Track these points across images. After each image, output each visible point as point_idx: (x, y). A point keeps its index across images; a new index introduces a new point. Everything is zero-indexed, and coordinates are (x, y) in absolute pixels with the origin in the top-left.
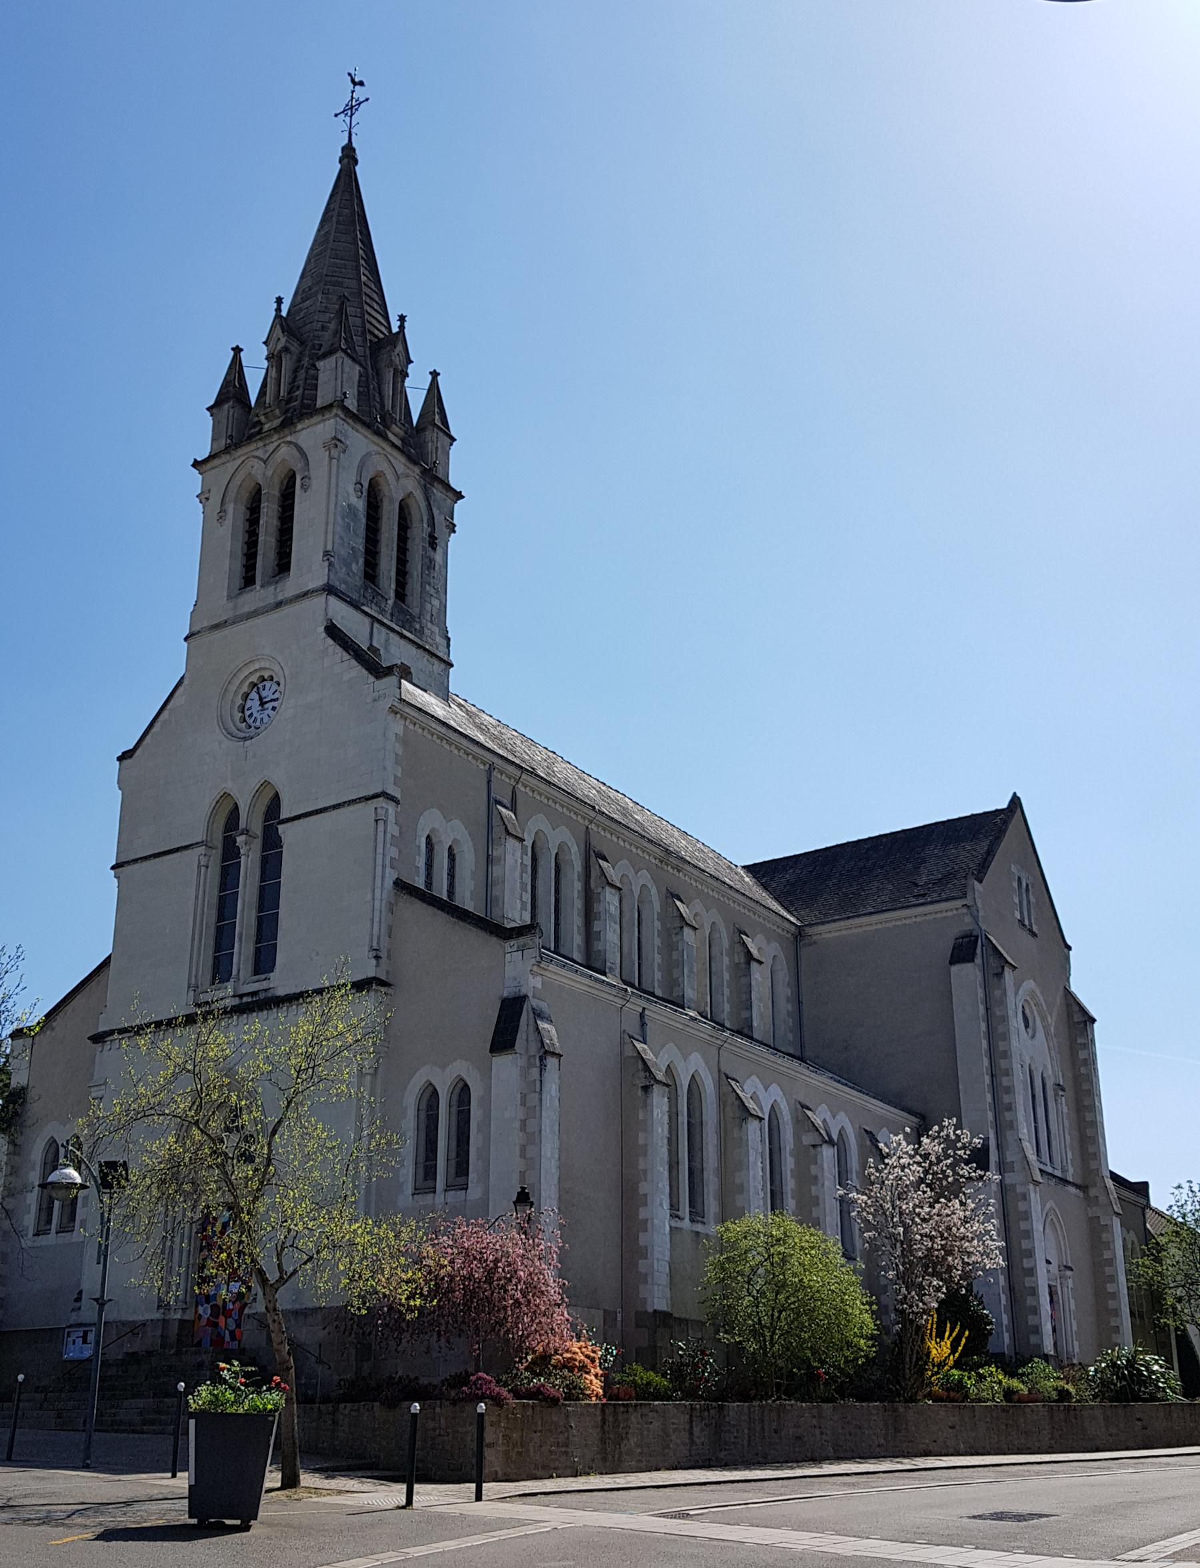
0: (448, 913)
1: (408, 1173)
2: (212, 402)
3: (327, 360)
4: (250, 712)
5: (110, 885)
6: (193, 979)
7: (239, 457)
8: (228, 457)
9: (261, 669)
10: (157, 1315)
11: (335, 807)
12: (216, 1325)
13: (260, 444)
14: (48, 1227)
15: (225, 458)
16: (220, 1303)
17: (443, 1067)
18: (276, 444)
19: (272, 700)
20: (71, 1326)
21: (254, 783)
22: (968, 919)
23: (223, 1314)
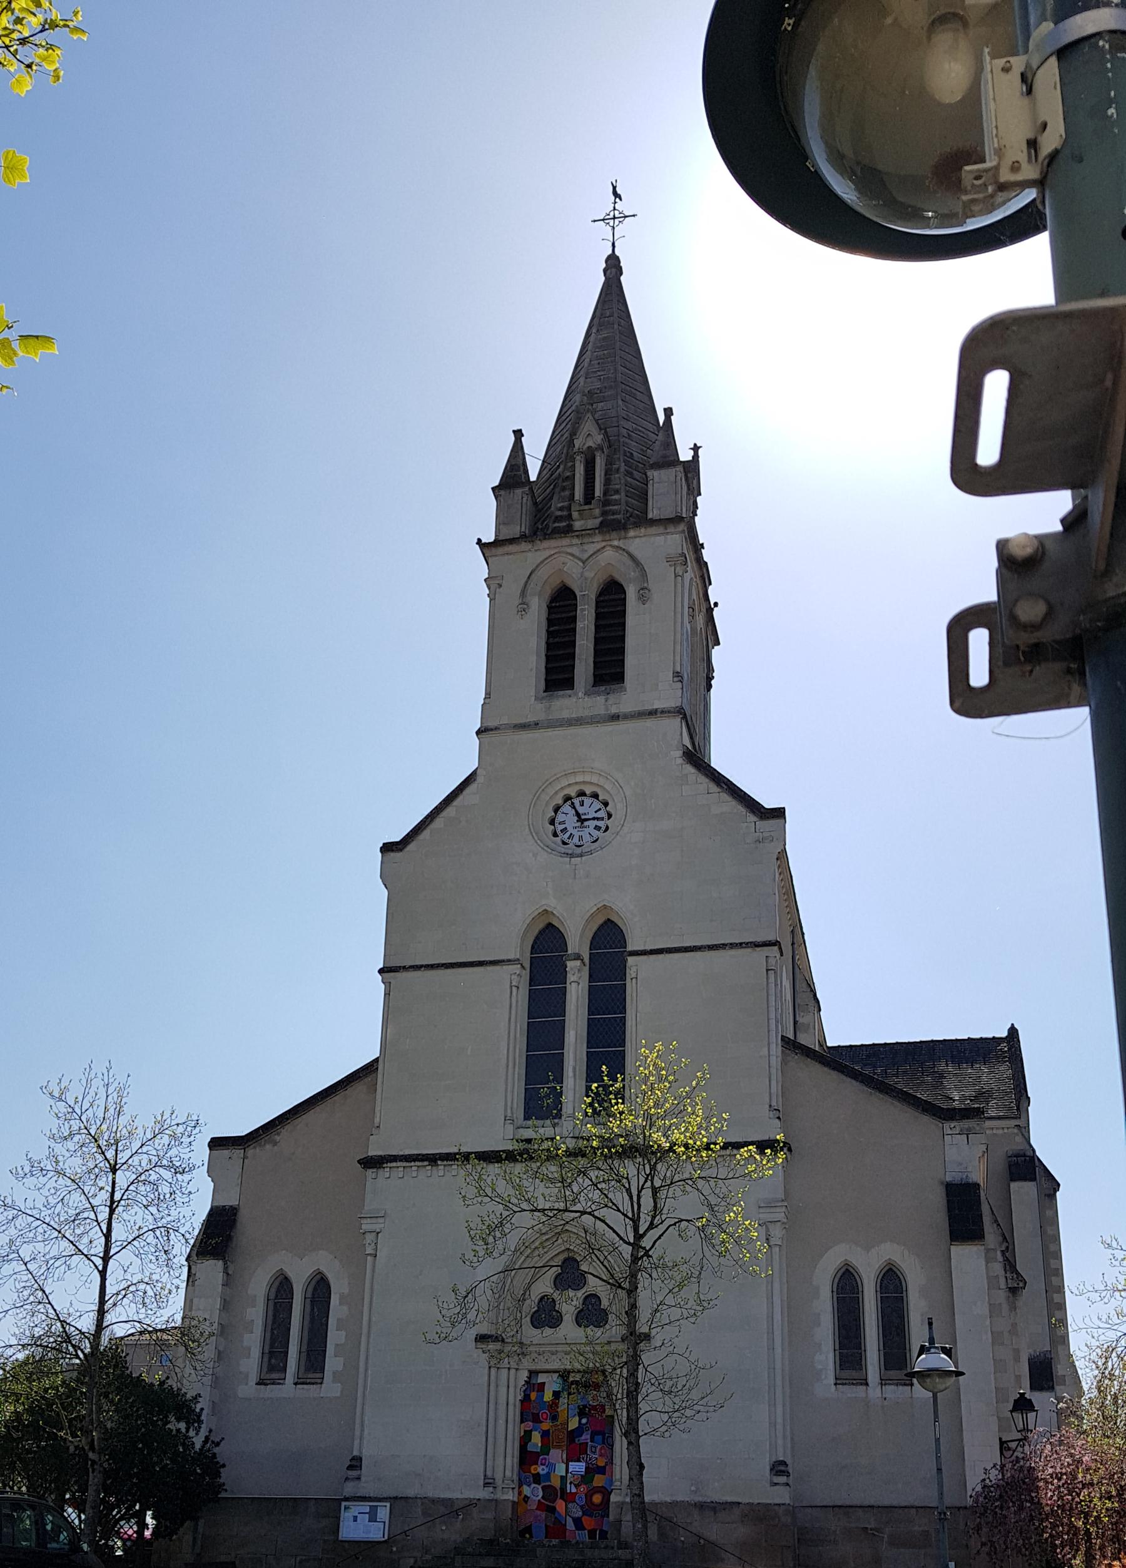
0: (862, 1082)
1: (826, 1358)
2: (497, 483)
3: (663, 472)
4: (562, 827)
5: (378, 987)
6: (509, 1111)
7: (545, 549)
8: (530, 546)
9: (584, 782)
10: (484, 1494)
11: (711, 948)
12: (553, 1510)
13: (575, 541)
14: (282, 1376)
15: (524, 546)
16: (556, 1483)
17: (868, 1249)
18: (599, 546)
19: (594, 819)
20: (346, 1499)
21: (588, 906)
22: (1019, 1139)
23: (562, 1498)
